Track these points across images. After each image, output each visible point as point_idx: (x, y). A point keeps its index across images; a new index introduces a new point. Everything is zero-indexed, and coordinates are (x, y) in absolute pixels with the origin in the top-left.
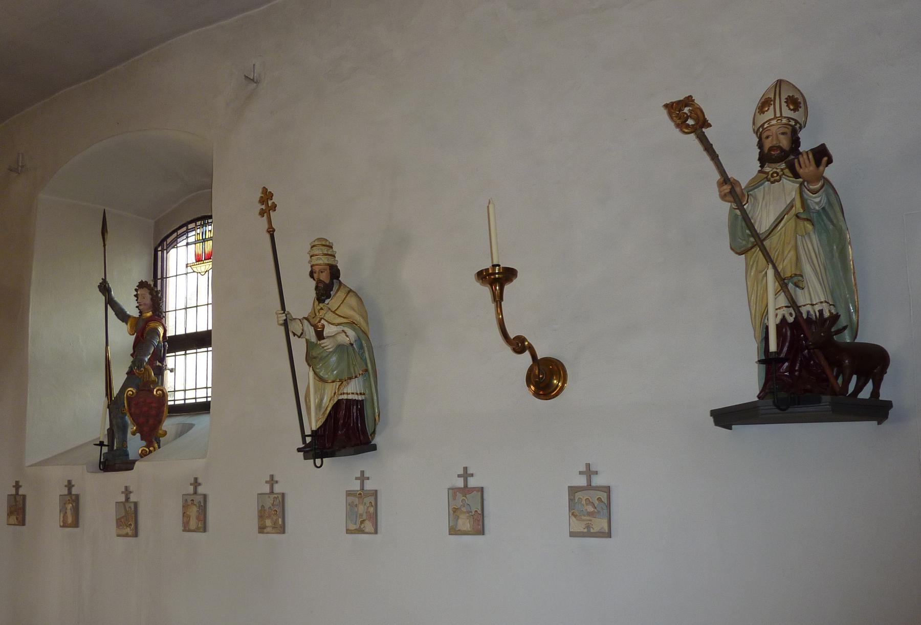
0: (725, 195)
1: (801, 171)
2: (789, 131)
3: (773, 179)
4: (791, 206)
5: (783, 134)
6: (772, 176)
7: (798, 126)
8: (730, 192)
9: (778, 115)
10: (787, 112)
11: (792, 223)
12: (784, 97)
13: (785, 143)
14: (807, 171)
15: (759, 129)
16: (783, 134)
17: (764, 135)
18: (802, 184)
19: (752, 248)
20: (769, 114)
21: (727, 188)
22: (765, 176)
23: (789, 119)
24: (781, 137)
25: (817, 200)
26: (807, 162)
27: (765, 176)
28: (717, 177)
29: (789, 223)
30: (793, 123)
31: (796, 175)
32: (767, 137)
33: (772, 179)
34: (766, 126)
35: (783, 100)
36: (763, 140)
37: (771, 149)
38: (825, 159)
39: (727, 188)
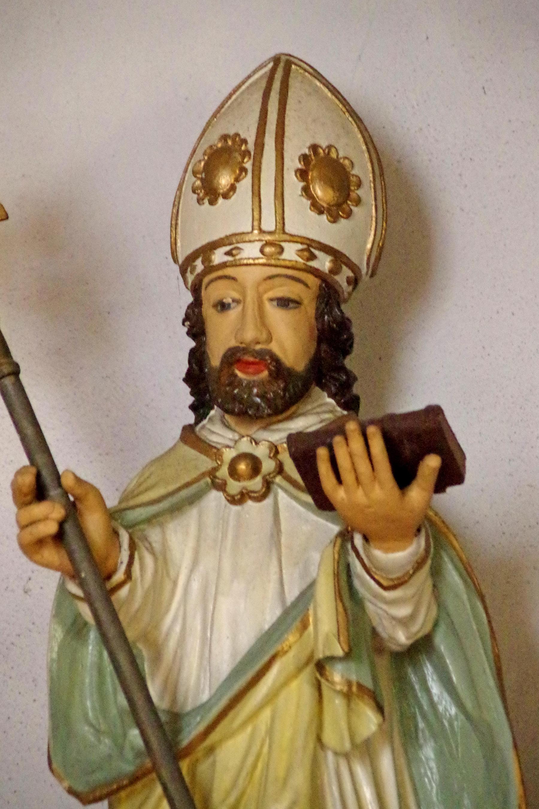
0: (40, 542)
1: (338, 495)
2: (307, 294)
3: (247, 481)
4: (296, 613)
5: (284, 303)
6: (233, 472)
7: (342, 279)
8: (59, 537)
9: (269, 222)
10: (304, 221)
11: (301, 689)
12: (295, 148)
13: (290, 340)
14: (360, 496)
15: (191, 259)
16: (284, 303)
17: (213, 293)
18: (346, 536)
19: (134, 779)
20: (232, 215)
21: (48, 515)
22: (206, 463)
23: (310, 247)
24: (277, 317)
25: (403, 611)
26: (363, 467)
27: (206, 463)
28: (22, 376)
29: (285, 698)
30: (324, 263)
31: (323, 503)
32: (222, 306)
33: (234, 487)
34: (219, 257)
35: (292, 163)
36: (208, 311)
37: (233, 357)
38: (432, 463)
39: (48, 515)
